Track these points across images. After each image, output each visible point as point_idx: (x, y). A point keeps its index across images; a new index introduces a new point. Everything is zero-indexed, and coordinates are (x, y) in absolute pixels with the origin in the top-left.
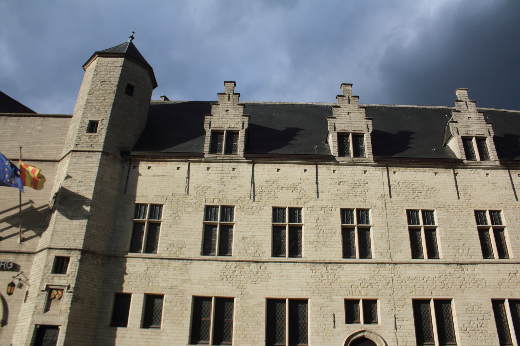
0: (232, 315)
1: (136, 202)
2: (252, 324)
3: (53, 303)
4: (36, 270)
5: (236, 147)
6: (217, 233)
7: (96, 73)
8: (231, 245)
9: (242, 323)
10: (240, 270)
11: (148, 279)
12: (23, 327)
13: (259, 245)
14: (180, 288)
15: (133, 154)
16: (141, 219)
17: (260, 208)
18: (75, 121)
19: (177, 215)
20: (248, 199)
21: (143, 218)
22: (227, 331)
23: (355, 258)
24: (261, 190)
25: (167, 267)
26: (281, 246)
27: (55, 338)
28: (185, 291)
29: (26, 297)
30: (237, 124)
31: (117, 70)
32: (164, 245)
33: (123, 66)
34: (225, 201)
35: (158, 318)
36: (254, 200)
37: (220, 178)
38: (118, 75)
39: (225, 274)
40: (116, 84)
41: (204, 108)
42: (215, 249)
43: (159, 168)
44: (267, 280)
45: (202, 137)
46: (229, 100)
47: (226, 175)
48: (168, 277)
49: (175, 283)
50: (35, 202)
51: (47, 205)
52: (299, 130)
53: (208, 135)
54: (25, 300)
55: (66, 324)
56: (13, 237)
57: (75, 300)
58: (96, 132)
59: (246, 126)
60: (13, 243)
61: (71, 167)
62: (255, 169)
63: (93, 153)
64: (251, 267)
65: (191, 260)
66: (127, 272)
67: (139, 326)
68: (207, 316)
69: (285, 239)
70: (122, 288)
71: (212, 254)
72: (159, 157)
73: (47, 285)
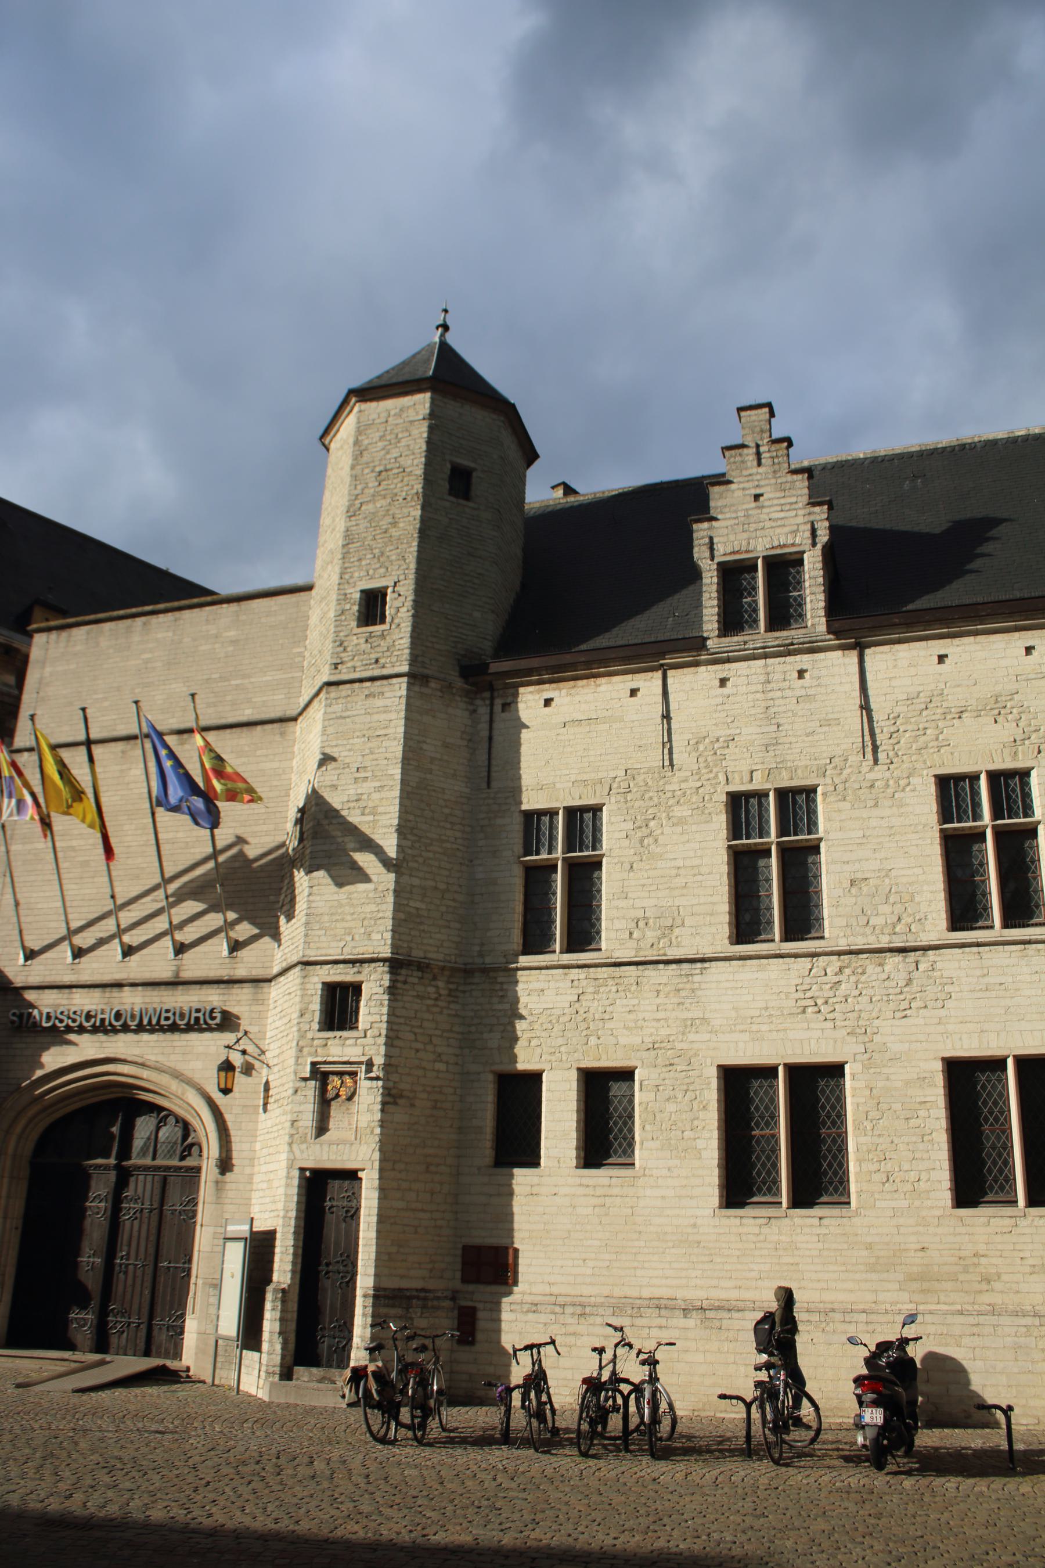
0: (841, 1116)
1: (524, 807)
2: (906, 1139)
3: (335, 1109)
4: (278, 1024)
5: (800, 605)
6: (773, 878)
7: (359, 451)
8: (819, 906)
9: (876, 1140)
10: (853, 979)
11: (584, 1025)
12: (272, 1176)
13: (906, 897)
14: (679, 1046)
15: (495, 667)
16: (544, 856)
17: (897, 782)
18: (323, 599)
19: (645, 831)
20: (855, 759)
21: (550, 853)
22: (830, 1165)
23: (992, 927)
24: (893, 729)
25: (634, 988)
26: (974, 895)
27: (354, 1204)
28: (696, 1055)
29: (266, 1097)
30: (795, 532)
31: (415, 432)
32: (618, 925)
33: (432, 415)
34: (785, 774)
35: (625, 1138)
36: (876, 761)
37: (764, 704)
38: (420, 446)
39: (809, 994)
40: (419, 471)
41: (685, 501)
42: (770, 923)
43: (577, 698)
44: (940, 1003)
45: (691, 588)
46: (759, 464)
47: (779, 694)
48: (641, 1016)
49: (664, 1032)
50: (249, 839)
51: (283, 845)
52: (995, 522)
53: (710, 580)
54: (265, 1104)
55: (377, 1165)
56: (210, 941)
57: (390, 1099)
58: (383, 621)
59: (823, 536)
60: (210, 959)
61: (330, 730)
62: (868, 665)
63: (385, 682)
64: (887, 968)
65: (703, 960)
66: (523, 1011)
67: (574, 1162)
68: (767, 1124)
69: (985, 873)
70: (514, 1059)
71: (763, 937)
72: (572, 666)
73: (314, 1064)
